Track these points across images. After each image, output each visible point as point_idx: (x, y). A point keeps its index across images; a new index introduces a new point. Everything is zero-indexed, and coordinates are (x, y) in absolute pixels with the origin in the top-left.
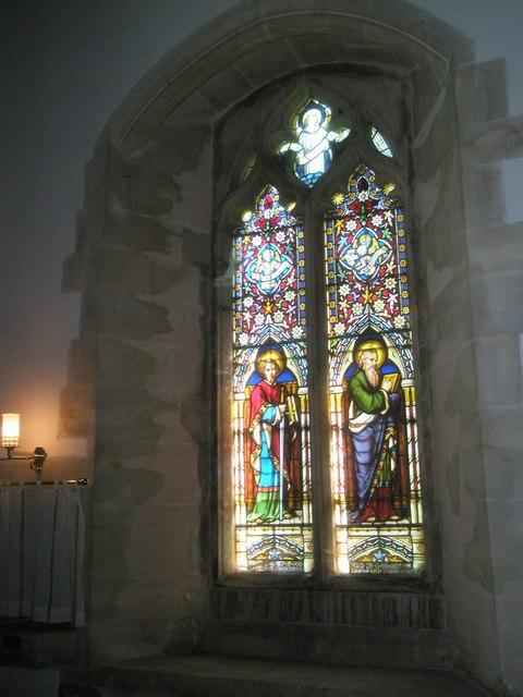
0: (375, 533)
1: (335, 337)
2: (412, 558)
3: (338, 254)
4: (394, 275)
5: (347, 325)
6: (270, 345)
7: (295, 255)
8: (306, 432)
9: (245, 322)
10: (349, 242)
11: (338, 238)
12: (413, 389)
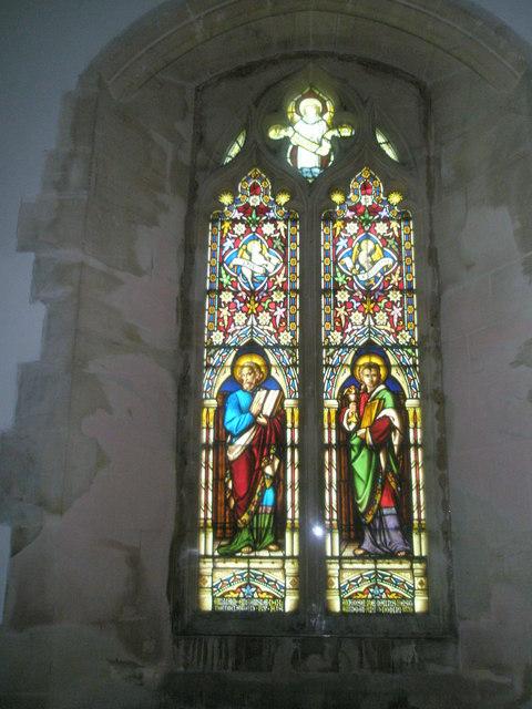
0: (372, 566)
1: (328, 347)
2: (413, 594)
3: (336, 257)
4: (283, 289)
5: (226, 334)
6: (251, 348)
7: (286, 253)
8: (330, 442)
9: (338, 319)
10: (350, 244)
11: (223, 240)
12: (418, 411)
